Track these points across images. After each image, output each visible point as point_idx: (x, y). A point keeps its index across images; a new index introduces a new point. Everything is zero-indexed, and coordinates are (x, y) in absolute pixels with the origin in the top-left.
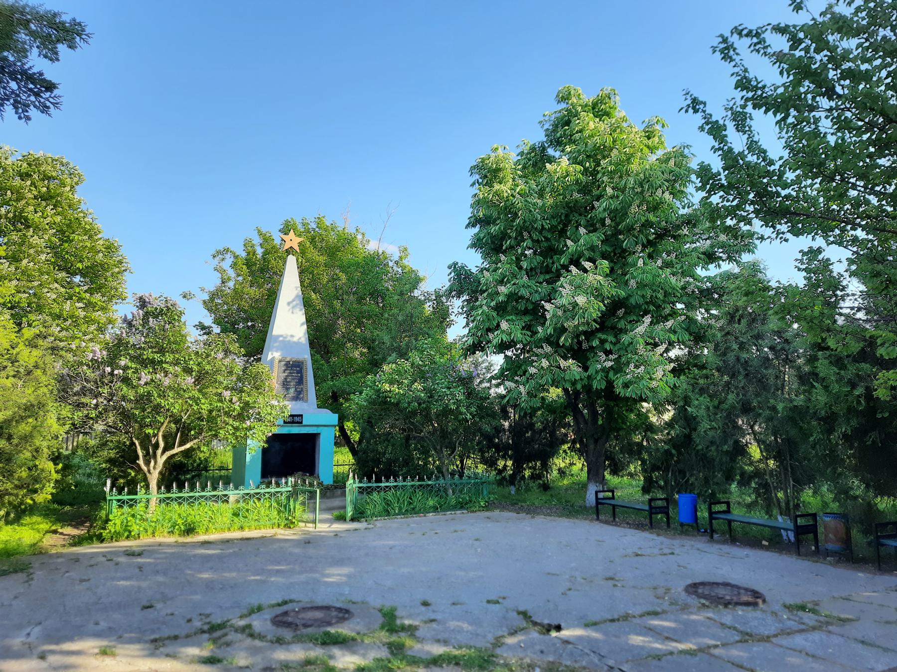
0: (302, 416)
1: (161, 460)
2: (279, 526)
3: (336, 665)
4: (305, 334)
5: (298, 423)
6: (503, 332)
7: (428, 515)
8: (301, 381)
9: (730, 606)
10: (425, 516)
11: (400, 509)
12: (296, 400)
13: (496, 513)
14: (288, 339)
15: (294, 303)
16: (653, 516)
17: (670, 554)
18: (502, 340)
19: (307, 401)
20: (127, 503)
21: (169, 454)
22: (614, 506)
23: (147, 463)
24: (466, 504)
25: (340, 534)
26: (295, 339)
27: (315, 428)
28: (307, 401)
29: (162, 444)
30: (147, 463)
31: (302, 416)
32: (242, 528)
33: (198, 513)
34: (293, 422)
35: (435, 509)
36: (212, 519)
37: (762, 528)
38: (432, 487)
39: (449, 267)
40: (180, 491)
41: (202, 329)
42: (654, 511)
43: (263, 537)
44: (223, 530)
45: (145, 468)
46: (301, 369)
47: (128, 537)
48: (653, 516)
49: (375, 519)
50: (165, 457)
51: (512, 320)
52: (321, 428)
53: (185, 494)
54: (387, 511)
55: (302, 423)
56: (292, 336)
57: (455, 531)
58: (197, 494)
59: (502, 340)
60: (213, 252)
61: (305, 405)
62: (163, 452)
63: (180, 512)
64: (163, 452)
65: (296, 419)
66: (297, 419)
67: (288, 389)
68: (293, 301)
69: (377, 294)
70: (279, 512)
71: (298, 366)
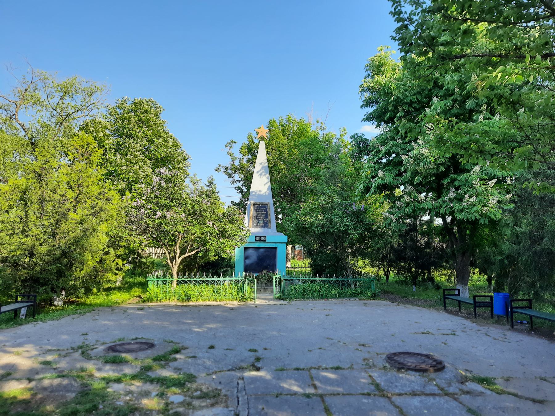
0: (266, 237)
1: (179, 261)
2: (237, 300)
3: (292, 389)
4: (268, 189)
5: (263, 241)
6: (380, 178)
7: (330, 299)
8: (266, 216)
9: (403, 370)
10: (328, 300)
11: (312, 295)
12: (264, 228)
13: (380, 302)
14: (258, 193)
15: (261, 171)
16: (477, 309)
17: (452, 334)
18: (378, 183)
19: (270, 228)
20: (181, 282)
21: (182, 257)
22: (459, 302)
23: (172, 262)
24: (358, 295)
25: (258, 307)
26: (262, 193)
27: (274, 244)
28: (270, 228)
29: (179, 252)
30: (172, 262)
31: (266, 237)
32: (216, 300)
33: (191, 289)
34: (261, 240)
35: (335, 296)
36: (200, 293)
37: (544, 320)
38: (339, 282)
39: (351, 138)
40: (183, 277)
41: (238, 189)
42: (490, 305)
43: (219, 305)
44: (205, 300)
45: (170, 264)
46: (267, 209)
47: (157, 300)
48: (477, 309)
49: (295, 299)
50: (181, 259)
51: (389, 170)
52: (278, 244)
53: (204, 279)
54: (304, 295)
55: (266, 241)
56: (260, 191)
57: (325, 309)
58: (192, 279)
59: (378, 183)
60: (226, 144)
61: (270, 230)
62: (179, 257)
63: (183, 289)
64: (179, 257)
65: (260, 238)
66: (263, 239)
67: (259, 221)
68: (260, 170)
69: (319, 161)
70: (238, 292)
71: (265, 207)
